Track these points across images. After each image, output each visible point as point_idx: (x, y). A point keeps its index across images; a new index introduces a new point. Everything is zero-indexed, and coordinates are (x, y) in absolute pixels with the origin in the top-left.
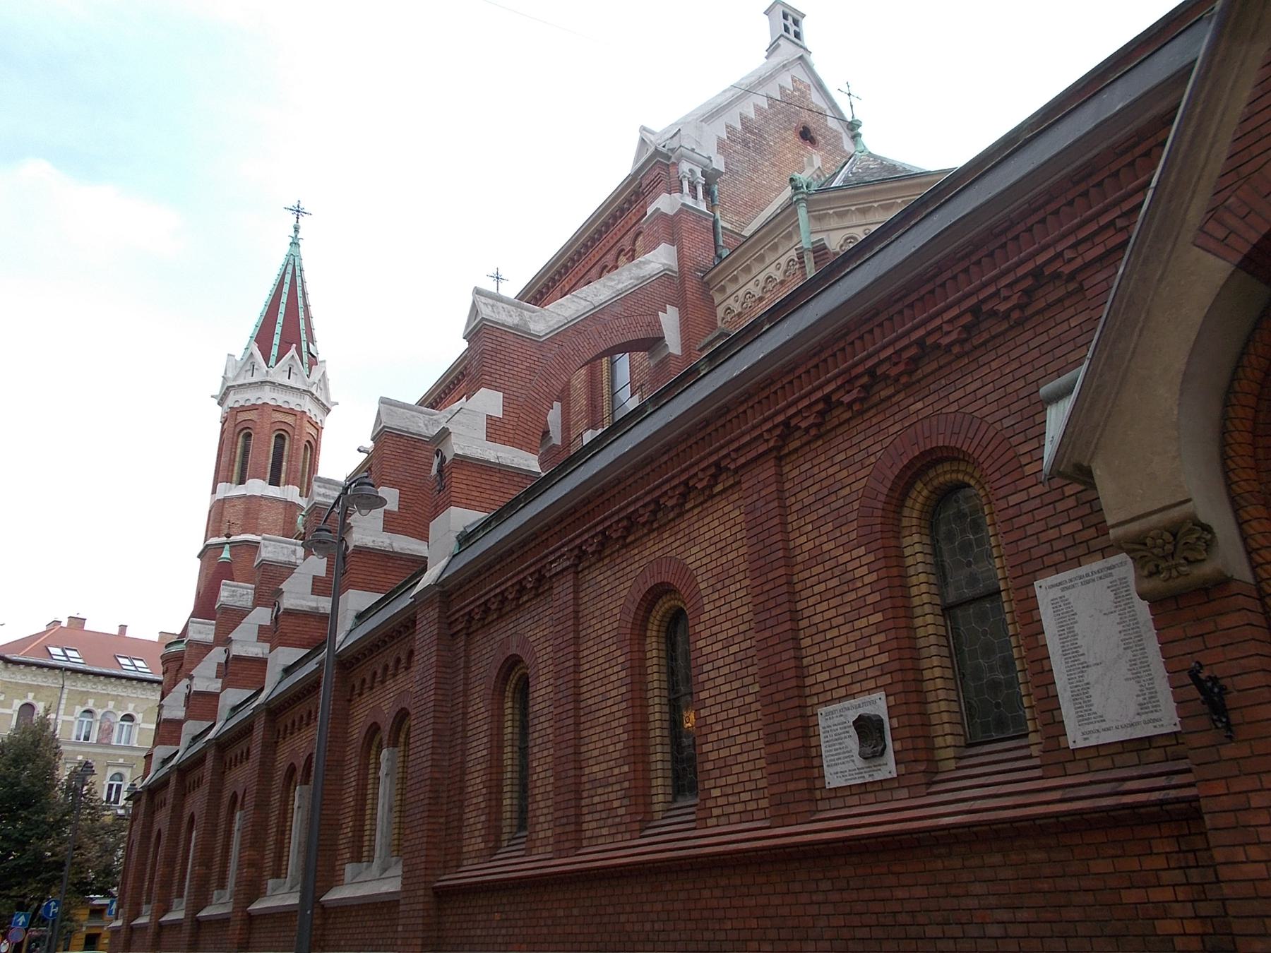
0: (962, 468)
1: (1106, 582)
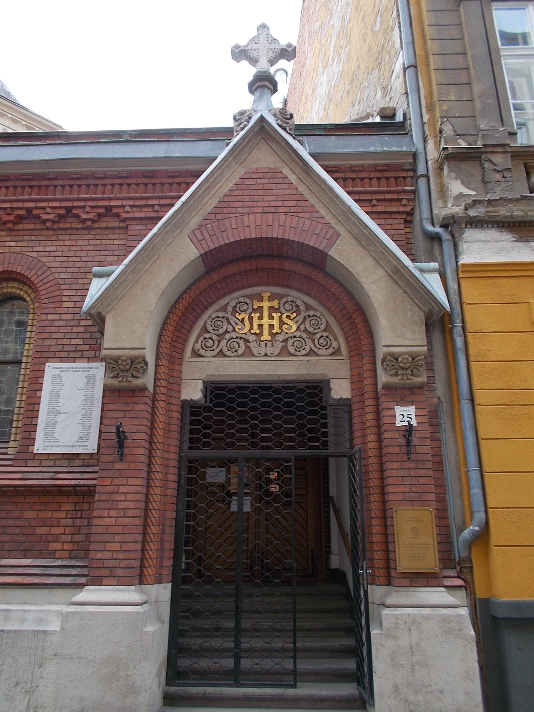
0: (25, 289)
1: (85, 374)
